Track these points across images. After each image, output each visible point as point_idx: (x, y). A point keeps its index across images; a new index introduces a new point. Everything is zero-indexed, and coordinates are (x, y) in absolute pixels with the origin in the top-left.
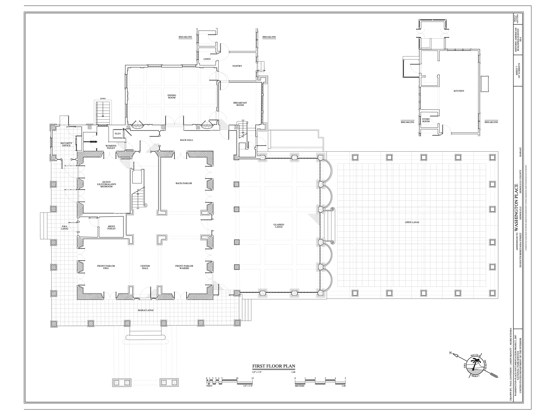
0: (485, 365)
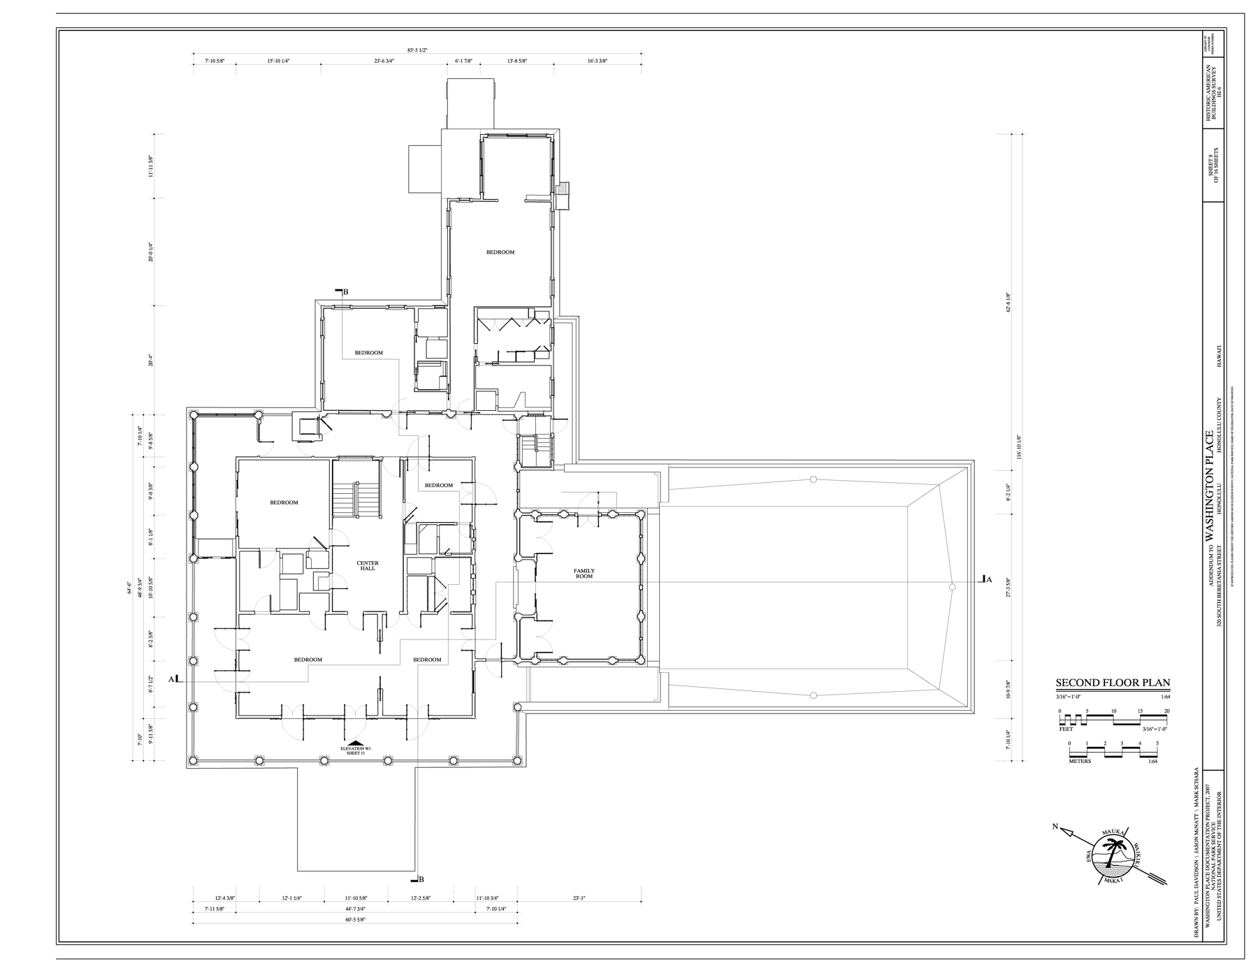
0: (1137, 854)
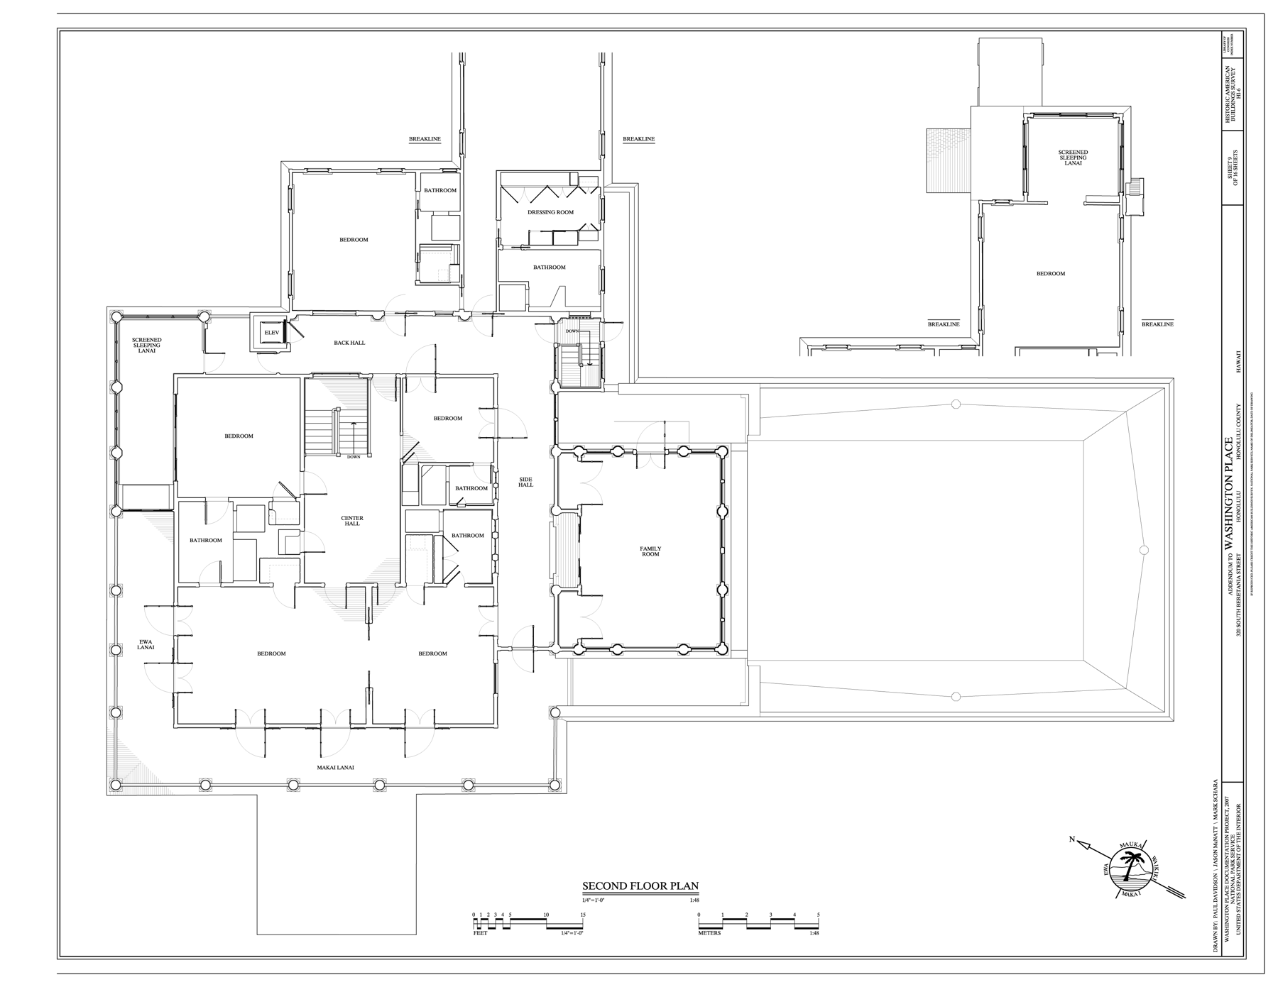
0: (1155, 868)
